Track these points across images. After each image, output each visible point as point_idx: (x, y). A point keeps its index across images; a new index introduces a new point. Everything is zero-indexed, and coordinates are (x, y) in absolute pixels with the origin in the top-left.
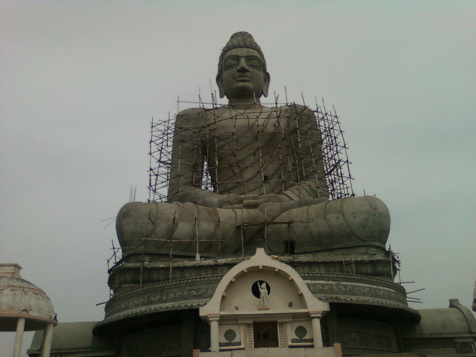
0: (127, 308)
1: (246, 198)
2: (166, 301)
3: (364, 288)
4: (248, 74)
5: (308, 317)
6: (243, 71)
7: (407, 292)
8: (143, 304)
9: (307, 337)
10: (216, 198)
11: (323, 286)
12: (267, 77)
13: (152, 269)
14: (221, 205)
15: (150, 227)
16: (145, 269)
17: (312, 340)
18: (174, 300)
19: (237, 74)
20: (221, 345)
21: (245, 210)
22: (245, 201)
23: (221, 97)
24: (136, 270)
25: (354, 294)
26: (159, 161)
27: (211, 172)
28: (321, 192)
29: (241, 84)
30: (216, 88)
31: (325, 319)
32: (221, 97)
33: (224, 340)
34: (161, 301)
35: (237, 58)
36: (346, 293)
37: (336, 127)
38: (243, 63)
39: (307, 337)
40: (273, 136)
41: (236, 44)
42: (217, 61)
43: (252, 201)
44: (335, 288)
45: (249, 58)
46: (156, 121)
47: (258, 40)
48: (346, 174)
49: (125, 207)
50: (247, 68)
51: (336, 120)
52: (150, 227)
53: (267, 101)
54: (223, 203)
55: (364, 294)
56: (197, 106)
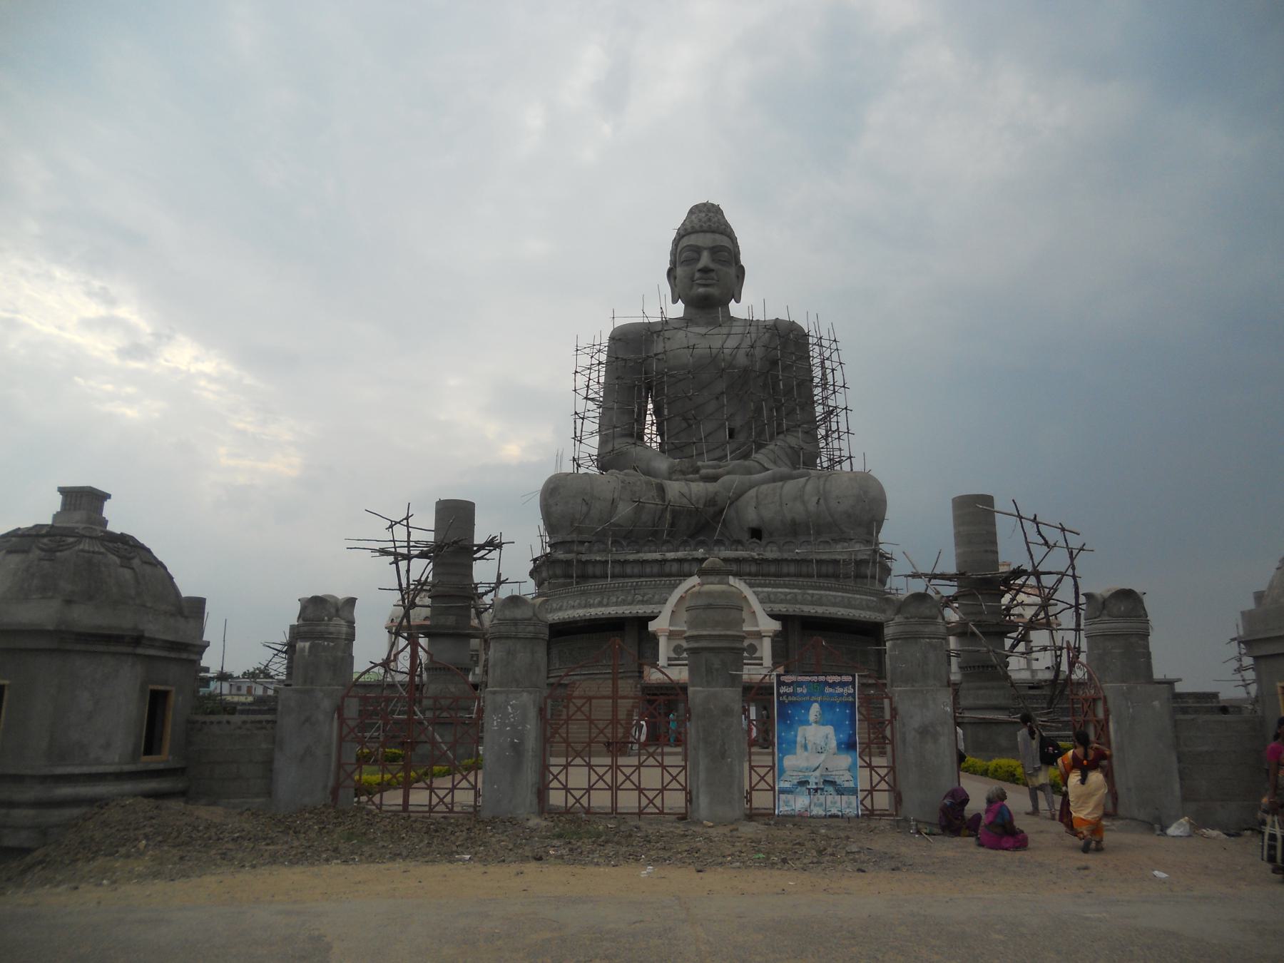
0: (560, 609)
1: (704, 467)
2: (607, 605)
3: (835, 597)
4: (713, 275)
5: (759, 635)
6: (705, 270)
7: (923, 591)
8: (580, 606)
9: (757, 655)
10: (663, 464)
11: (786, 594)
12: (741, 272)
13: (587, 562)
14: (671, 474)
15: (585, 509)
16: (579, 561)
17: (761, 659)
18: (617, 604)
19: (697, 275)
20: (669, 659)
21: (702, 484)
22: (703, 471)
23: (675, 301)
24: (568, 563)
25: (821, 605)
26: (586, 398)
27: (657, 412)
28: (805, 458)
29: (701, 290)
30: (666, 289)
31: (777, 638)
32: (675, 301)
33: (674, 656)
34: (600, 604)
35: (697, 250)
36: (812, 603)
37: (835, 357)
38: (705, 260)
39: (757, 655)
40: (746, 370)
41: (697, 227)
42: (669, 247)
43: (711, 471)
44: (799, 597)
45: (715, 250)
46: (581, 345)
47: (731, 217)
48: (843, 428)
49: (550, 480)
50: (712, 266)
51: (834, 346)
52: (585, 509)
53: (736, 310)
54: (674, 472)
55: (834, 605)
56: (641, 320)
